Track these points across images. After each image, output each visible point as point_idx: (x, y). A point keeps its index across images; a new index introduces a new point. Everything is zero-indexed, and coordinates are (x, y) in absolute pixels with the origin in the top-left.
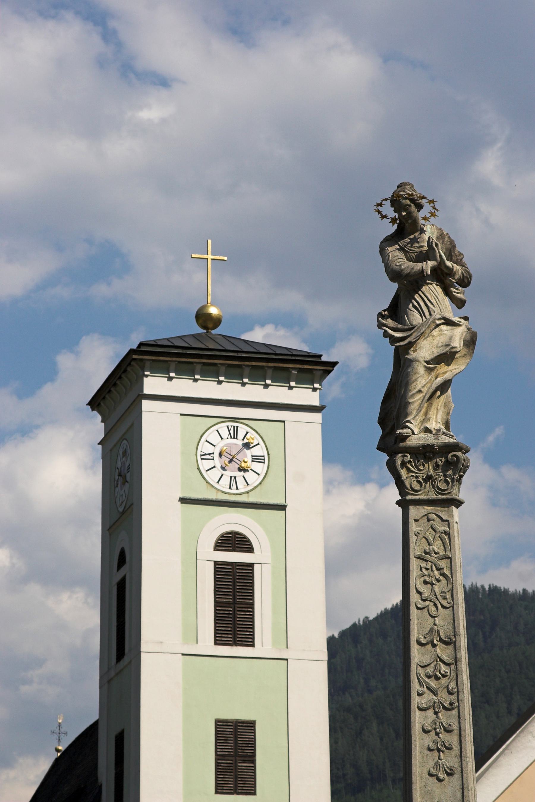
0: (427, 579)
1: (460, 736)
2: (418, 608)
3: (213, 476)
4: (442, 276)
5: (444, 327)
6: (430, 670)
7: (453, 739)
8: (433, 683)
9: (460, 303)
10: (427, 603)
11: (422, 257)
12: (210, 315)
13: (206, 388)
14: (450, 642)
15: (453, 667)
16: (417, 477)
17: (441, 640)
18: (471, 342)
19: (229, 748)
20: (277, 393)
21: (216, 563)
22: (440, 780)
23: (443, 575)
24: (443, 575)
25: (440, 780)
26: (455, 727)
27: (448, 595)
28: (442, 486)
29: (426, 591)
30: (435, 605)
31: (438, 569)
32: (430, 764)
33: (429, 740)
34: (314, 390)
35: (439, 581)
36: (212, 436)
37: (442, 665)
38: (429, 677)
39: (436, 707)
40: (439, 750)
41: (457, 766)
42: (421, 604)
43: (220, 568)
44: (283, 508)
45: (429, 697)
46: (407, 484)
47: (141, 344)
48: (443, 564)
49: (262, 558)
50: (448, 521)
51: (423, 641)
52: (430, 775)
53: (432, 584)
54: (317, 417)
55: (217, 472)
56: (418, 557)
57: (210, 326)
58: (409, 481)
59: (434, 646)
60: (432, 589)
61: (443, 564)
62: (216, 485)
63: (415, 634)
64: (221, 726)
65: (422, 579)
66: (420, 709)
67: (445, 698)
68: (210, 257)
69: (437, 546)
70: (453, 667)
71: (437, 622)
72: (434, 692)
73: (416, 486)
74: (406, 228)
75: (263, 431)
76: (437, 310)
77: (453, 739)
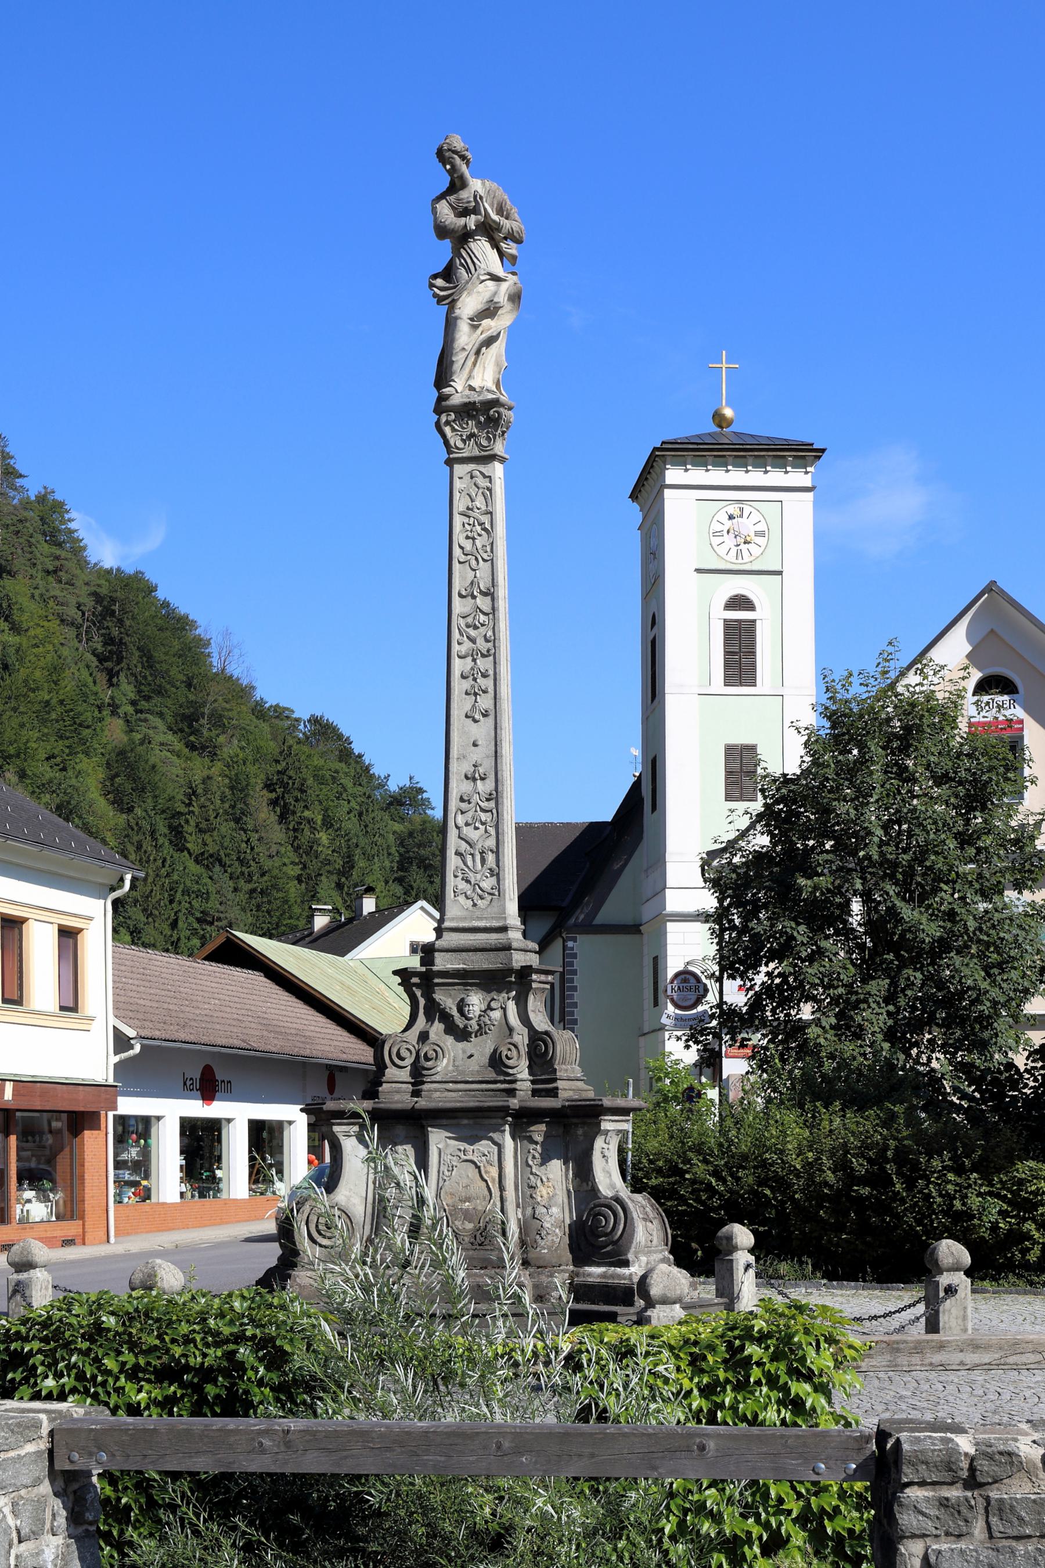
0: (470, 534)
1: (495, 680)
2: (460, 562)
3: (722, 551)
4: (489, 230)
5: (490, 283)
6: (470, 620)
7: (487, 683)
8: (472, 632)
10: (469, 557)
12: (724, 415)
13: (716, 476)
14: (490, 594)
15: (491, 616)
16: (461, 436)
17: (481, 592)
18: (515, 298)
19: (736, 766)
20: (775, 477)
21: (725, 620)
22: (475, 721)
23: (485, 529)
24: (485, 529)
25: (475, 721)
26: (491, 672)
27: (488, 549)
28: (484, 443)
29: (468, 545)
30: (476, 559)
31: (480, 524)
32: (468, 707)
33: (467, 685)
34: (807, 473)
35: (480, 535)
37: (481, 616)
38: (468, 626)
39: (473, 655)
40: (476, 694)
41: (492, 707)
42: (463, 558)
43: (728, 625)
44: (780, 573)
45: (467, 645)
46: (452, 443)
47: (663, 443)
48: (485, 519)
49: (764, 617)
50: (490, 477)
51: (464, 593)
52: (467, 716)
53: (474, 539)
54: (810, 496)
56: (461, 514)
57: (724, 425)
58: (454, 440)
59: (474, 597)
60: (474, 543)
61: (485, 519)
62: (725, 557)
64: (730, 751)
65: (465, 535)
66: (459, 657)
68: (724, 365)
69: (480, 502)
70: (491, 616)
71: (478, 575)
72: (473, 640)
73: (460, 444)
76: (483, 266)
77: (487, 683)
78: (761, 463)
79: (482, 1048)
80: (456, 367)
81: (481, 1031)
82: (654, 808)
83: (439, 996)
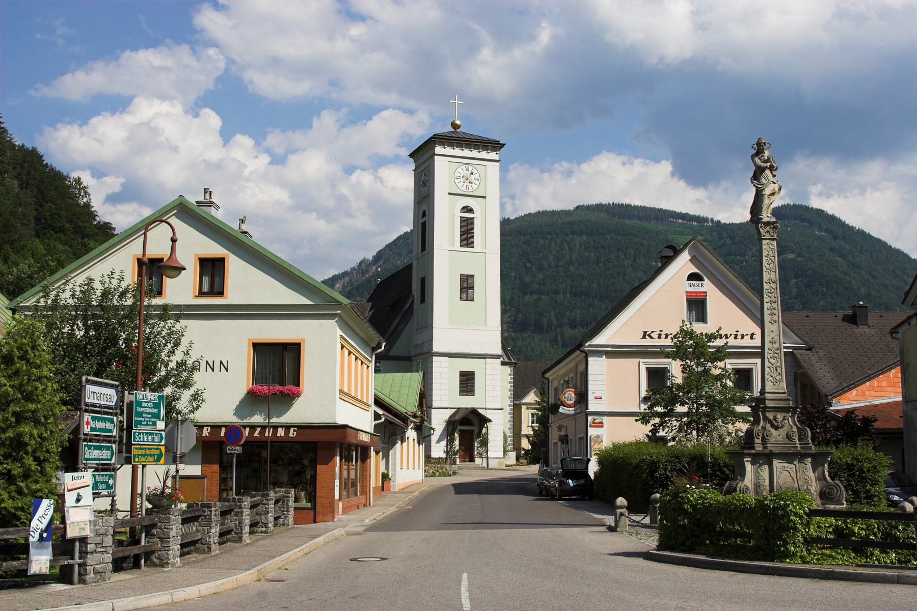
3: (460, 185)
9: (774, 176)
11: (765, 162)
20: (483, 154)
33: (769, 312)
36: (460, 170)
39: (771, 302)
49: (477, 216)
54: (498, 164)
55: (462, 183)
63: (765, 279)
67: (774, 300)
74: (759, 152)
75: (478, 169)
77: (776, 312)
78: (477, 148)
79: (782, 433)
80: (765, 207)
81: (782, 427)
82: (423, 300)
83: (768, 414)
